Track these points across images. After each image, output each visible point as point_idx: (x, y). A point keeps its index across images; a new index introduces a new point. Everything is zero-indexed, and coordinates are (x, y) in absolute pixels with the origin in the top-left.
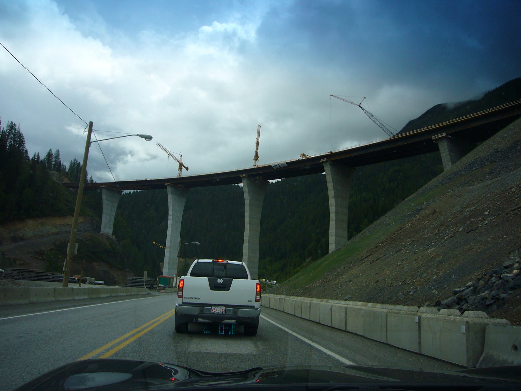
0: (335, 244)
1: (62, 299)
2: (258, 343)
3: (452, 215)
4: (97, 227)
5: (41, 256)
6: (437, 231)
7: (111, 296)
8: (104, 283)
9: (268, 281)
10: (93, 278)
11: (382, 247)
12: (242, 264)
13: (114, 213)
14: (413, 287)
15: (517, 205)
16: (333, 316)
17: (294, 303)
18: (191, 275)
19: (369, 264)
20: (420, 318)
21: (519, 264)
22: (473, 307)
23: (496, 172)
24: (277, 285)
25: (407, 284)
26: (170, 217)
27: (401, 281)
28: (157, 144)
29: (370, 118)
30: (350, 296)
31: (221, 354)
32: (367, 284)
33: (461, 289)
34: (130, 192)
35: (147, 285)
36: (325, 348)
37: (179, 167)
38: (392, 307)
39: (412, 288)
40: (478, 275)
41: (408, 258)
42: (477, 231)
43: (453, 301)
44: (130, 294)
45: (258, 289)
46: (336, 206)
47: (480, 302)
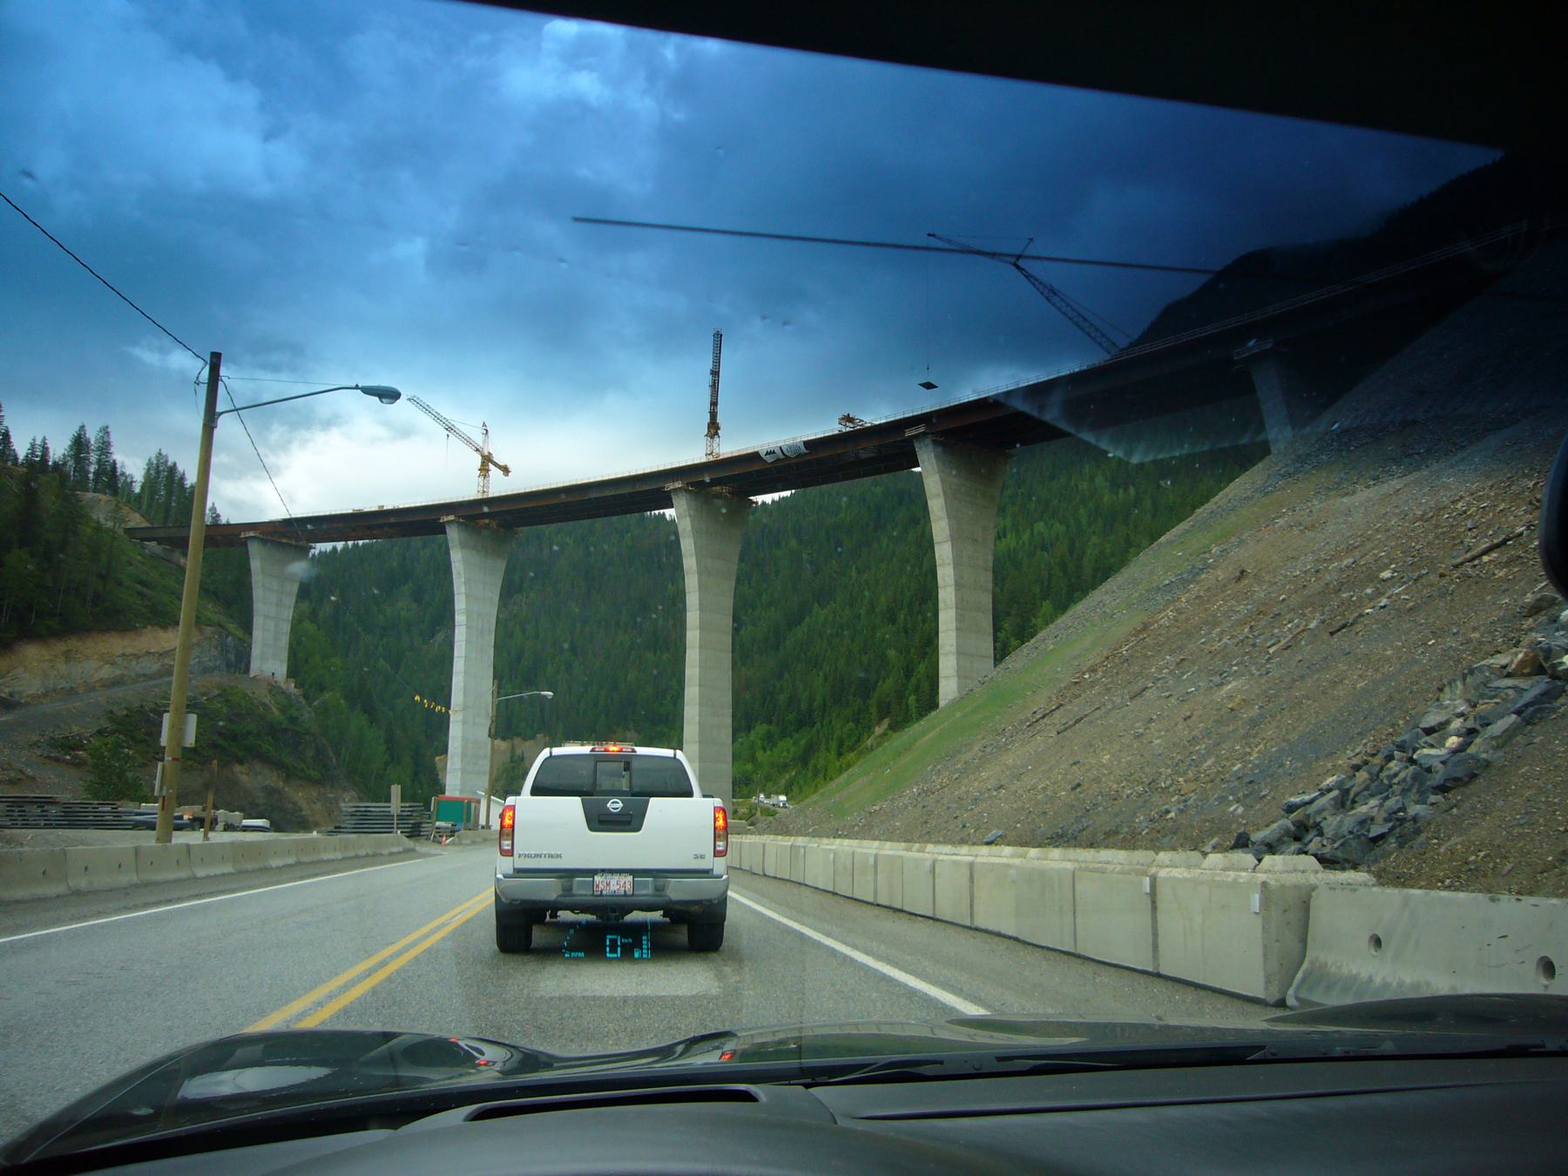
0: (956, 679)
1: (158, 877)
2: (725, 968)
3: (1289, 583)
4: (240, 659)
5: (69, 755)
6: (1246, 630)
7: (299, 864)
8: (271, 826)
9: (762, 796)
10: (237, 813)
11: (1092, 684)
12: (675, 755)
13: (288, 614)
14: (1177, 797)
15: (1469, 549)
16: (937, 887)
17: (832, 856)
18: (536, 791)
19: (1053, 734)
20: (1154, 880)
21: (1465, 720)
22: (1336, 845)
23: (1418, 454)
24: (791, 807)
25: (1159, 790)
26: (460, 618)
27: (1143, 782)
28: (409, 399)
29: (1049, 301)
30: (1000, 833)
31: (625, 1000)
32: (1047, 795)
33: (1307, 798)
34: (335, 548)
35: (400, 826)
36: (906, 972)
37: (482, 465)
38: (1087, 855)
39: (1173, 800)
40: (1354, 756)
41: (1165, 715)
42: (1358, 627)
43: (1282, 832)
44: (352, 854)
45: (720, 823)
46: (957, 564)
47: (1355, 830)
